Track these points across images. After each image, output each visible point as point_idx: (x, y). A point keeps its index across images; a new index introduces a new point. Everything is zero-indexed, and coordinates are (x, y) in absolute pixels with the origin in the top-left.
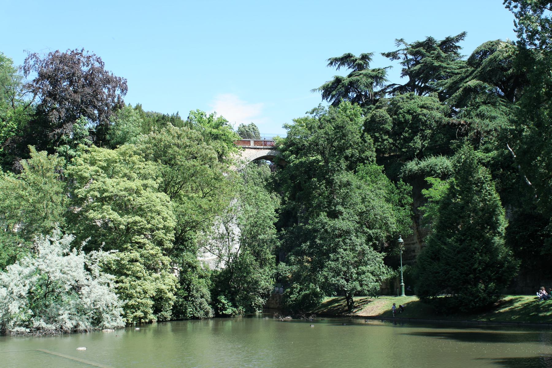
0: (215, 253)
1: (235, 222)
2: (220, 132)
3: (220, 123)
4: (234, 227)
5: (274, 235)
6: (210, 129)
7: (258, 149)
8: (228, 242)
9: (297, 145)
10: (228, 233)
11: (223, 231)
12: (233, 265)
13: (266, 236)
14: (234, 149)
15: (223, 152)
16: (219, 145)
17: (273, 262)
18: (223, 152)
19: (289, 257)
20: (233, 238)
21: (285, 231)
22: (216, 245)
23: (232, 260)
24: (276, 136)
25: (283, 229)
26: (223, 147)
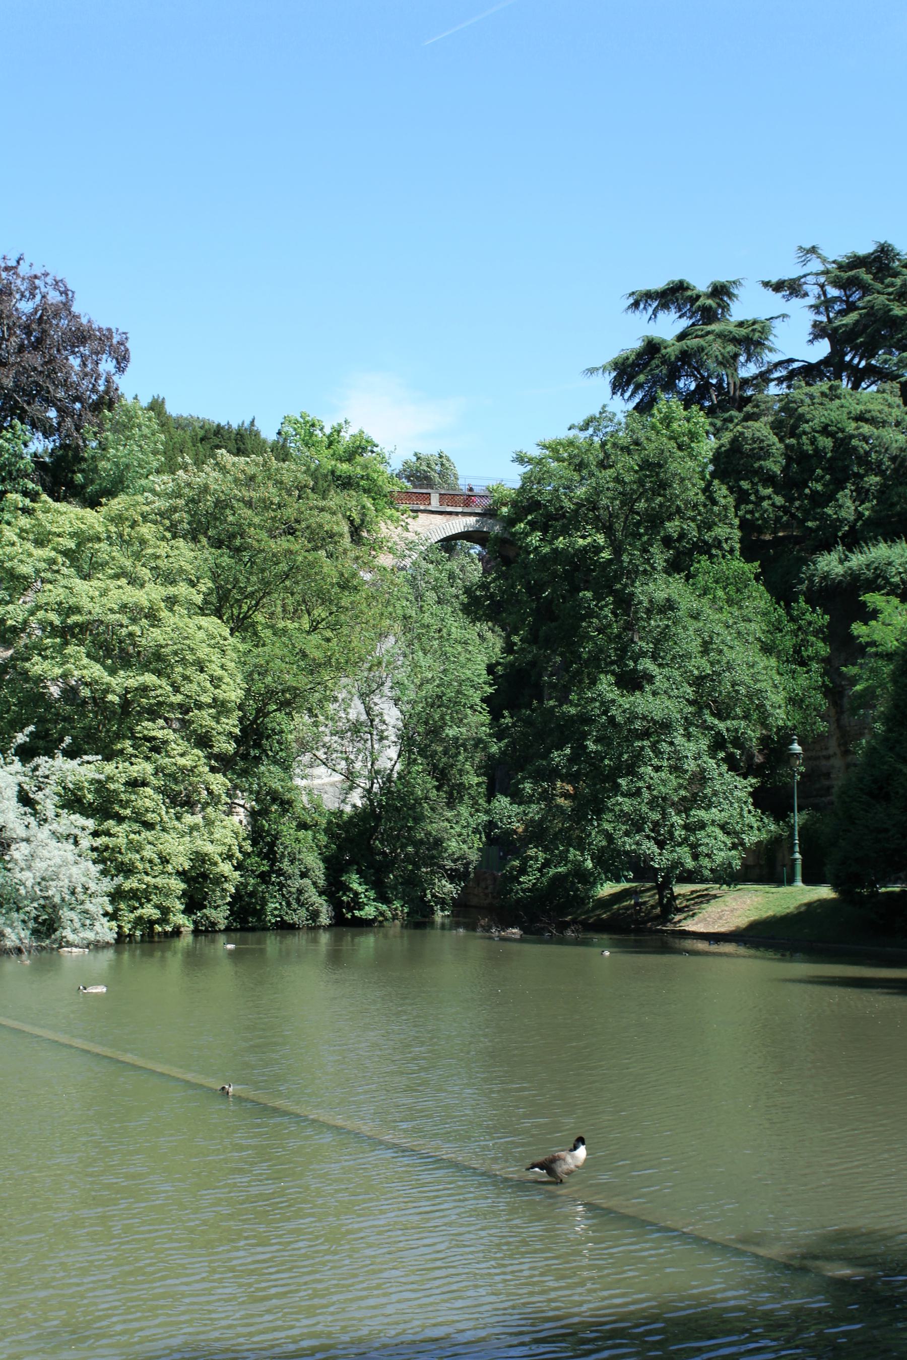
0: (338, 767)
1: (389, 694)
3: (358, 447)
5: (484, 728)
6: (333, 463)
7: (450, 513)
8: (369, 742)
10: (372, 721)
13: (464, 730)
14: (389, 512)
15: (363, 521)
16: (354, 503)
17: (479, 793)
18: (363, 521)
21: (512, 717)
23: (381, 788)
25: (506, 713)
26: (364, 507)
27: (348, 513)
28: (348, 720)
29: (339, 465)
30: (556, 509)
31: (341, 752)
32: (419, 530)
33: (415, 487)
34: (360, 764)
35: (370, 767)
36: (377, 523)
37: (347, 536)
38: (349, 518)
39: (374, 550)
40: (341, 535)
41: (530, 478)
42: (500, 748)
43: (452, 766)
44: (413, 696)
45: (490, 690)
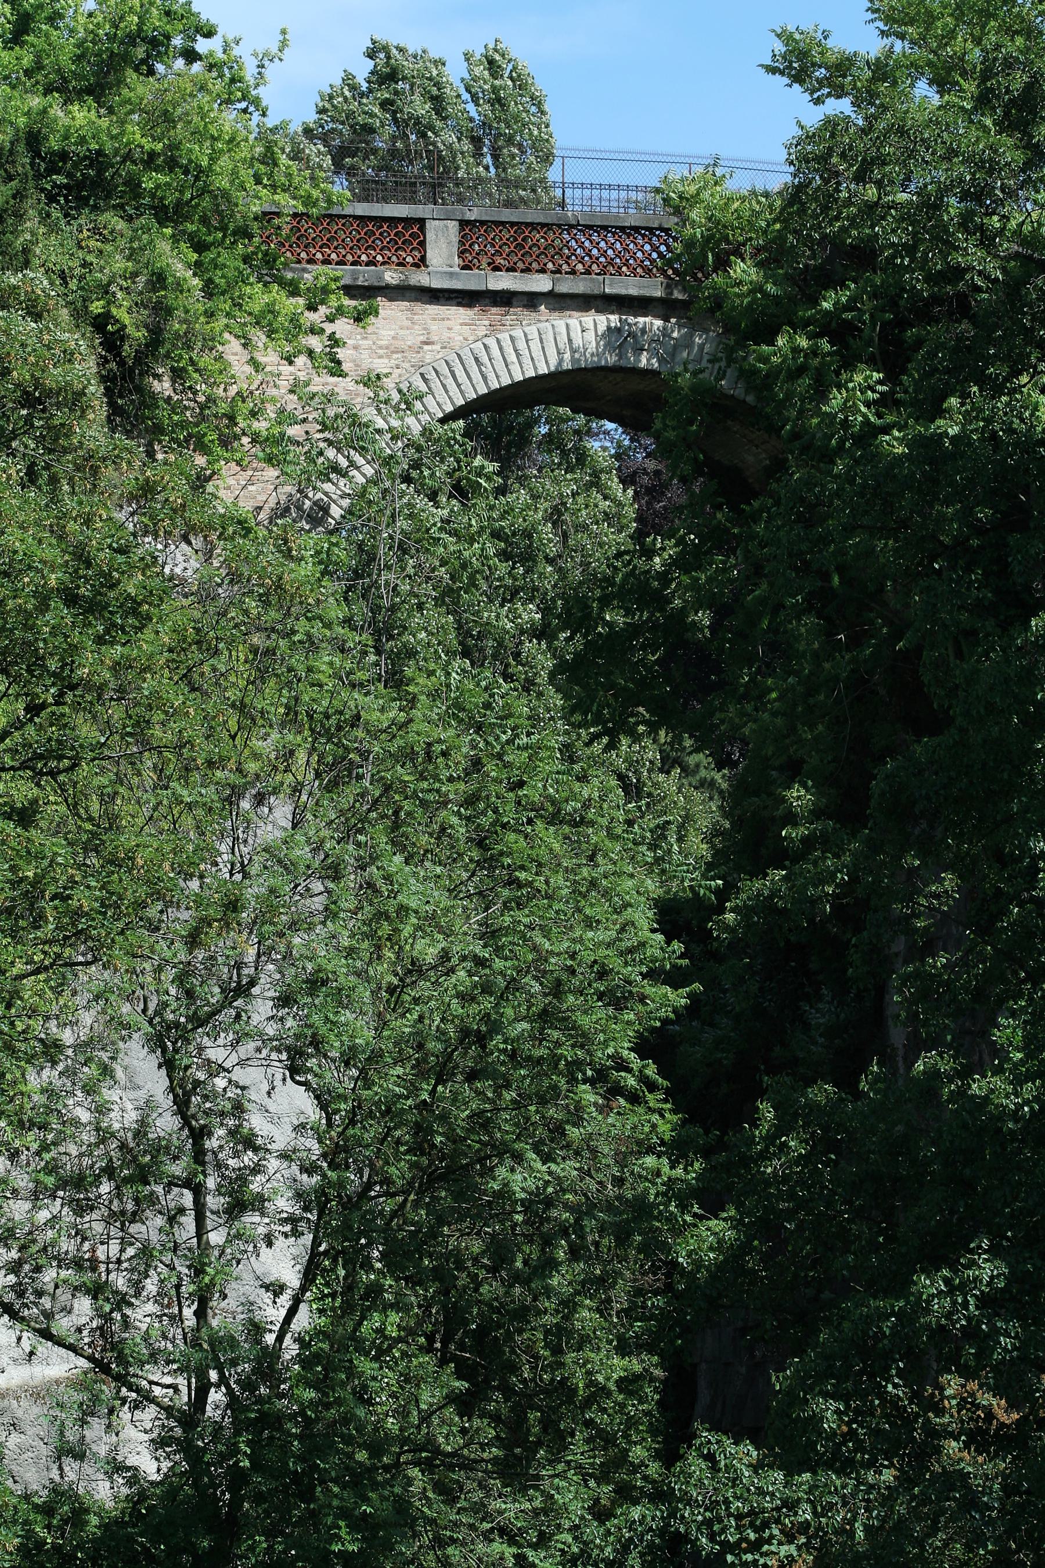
0: (62, 1325)
2: (135, 134)
3: (132, 39)
4: (251, 1076)
5: (650, 1161)
6: (36, 102)
7: (504, 299)
8: (188, 1221)
10: (198, 1135)
11: (148, 1106)
13: (568, 1168)
15: (156, 334)
16: (120, 264)
17: (631, 1423)
18: (156, 334)
20: (242, 1178)
22: (67, 1246)
26: (159, 280)
27: (97, 307)
28: (104, 1135)
29: (56, 111)
31: (78, 1264)
32: (381, 366)
33: (366, 192)
34: (151, 1307)
35: (190, 1321)
36: (210, 342)
38: (100, 323)
39: (202, 448)
40: (76, 400)
43: (522, 1314)
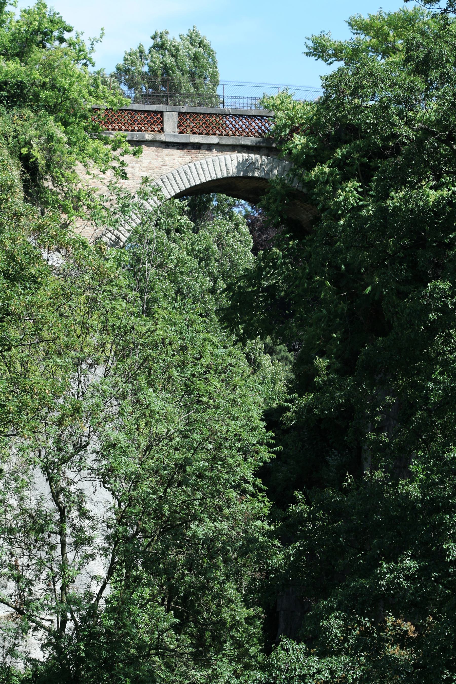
1: (95, 465)
3: (37, 32)
5: (259, 523)
7: (198, 146)
8: (59, 550)
9: (365, 136)
11: (40, 499)
12: (78, 649)
13: (224, 526)
14: (92, 145)
17: (251, 636)
19: (319, 617)
21: (308, 503)
23: (77, 628)
24: (275, 93)
25: (299, 495)
26: (50, 138)
30: (384, 139)
35: (58, 591)
37: (19, 187)
41: (337, 86)
42: (287, 557)
44: (134, 467)
45: (266, 455)
